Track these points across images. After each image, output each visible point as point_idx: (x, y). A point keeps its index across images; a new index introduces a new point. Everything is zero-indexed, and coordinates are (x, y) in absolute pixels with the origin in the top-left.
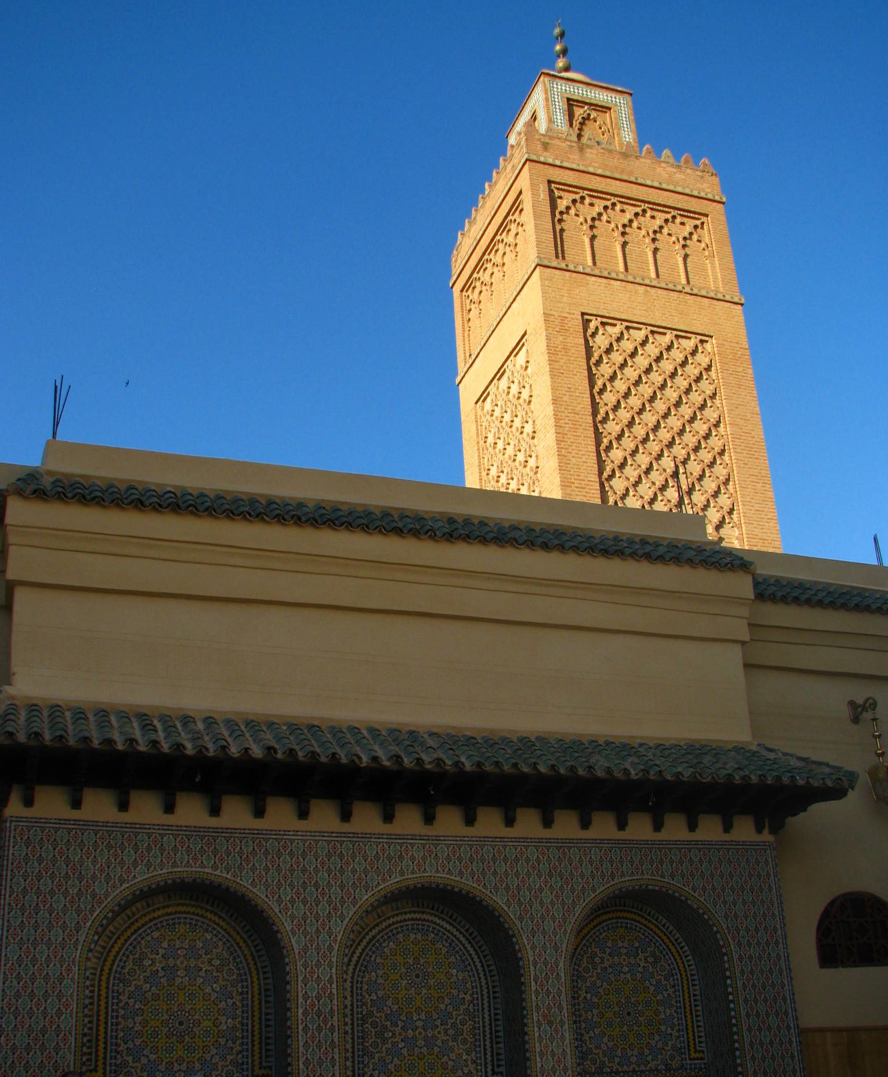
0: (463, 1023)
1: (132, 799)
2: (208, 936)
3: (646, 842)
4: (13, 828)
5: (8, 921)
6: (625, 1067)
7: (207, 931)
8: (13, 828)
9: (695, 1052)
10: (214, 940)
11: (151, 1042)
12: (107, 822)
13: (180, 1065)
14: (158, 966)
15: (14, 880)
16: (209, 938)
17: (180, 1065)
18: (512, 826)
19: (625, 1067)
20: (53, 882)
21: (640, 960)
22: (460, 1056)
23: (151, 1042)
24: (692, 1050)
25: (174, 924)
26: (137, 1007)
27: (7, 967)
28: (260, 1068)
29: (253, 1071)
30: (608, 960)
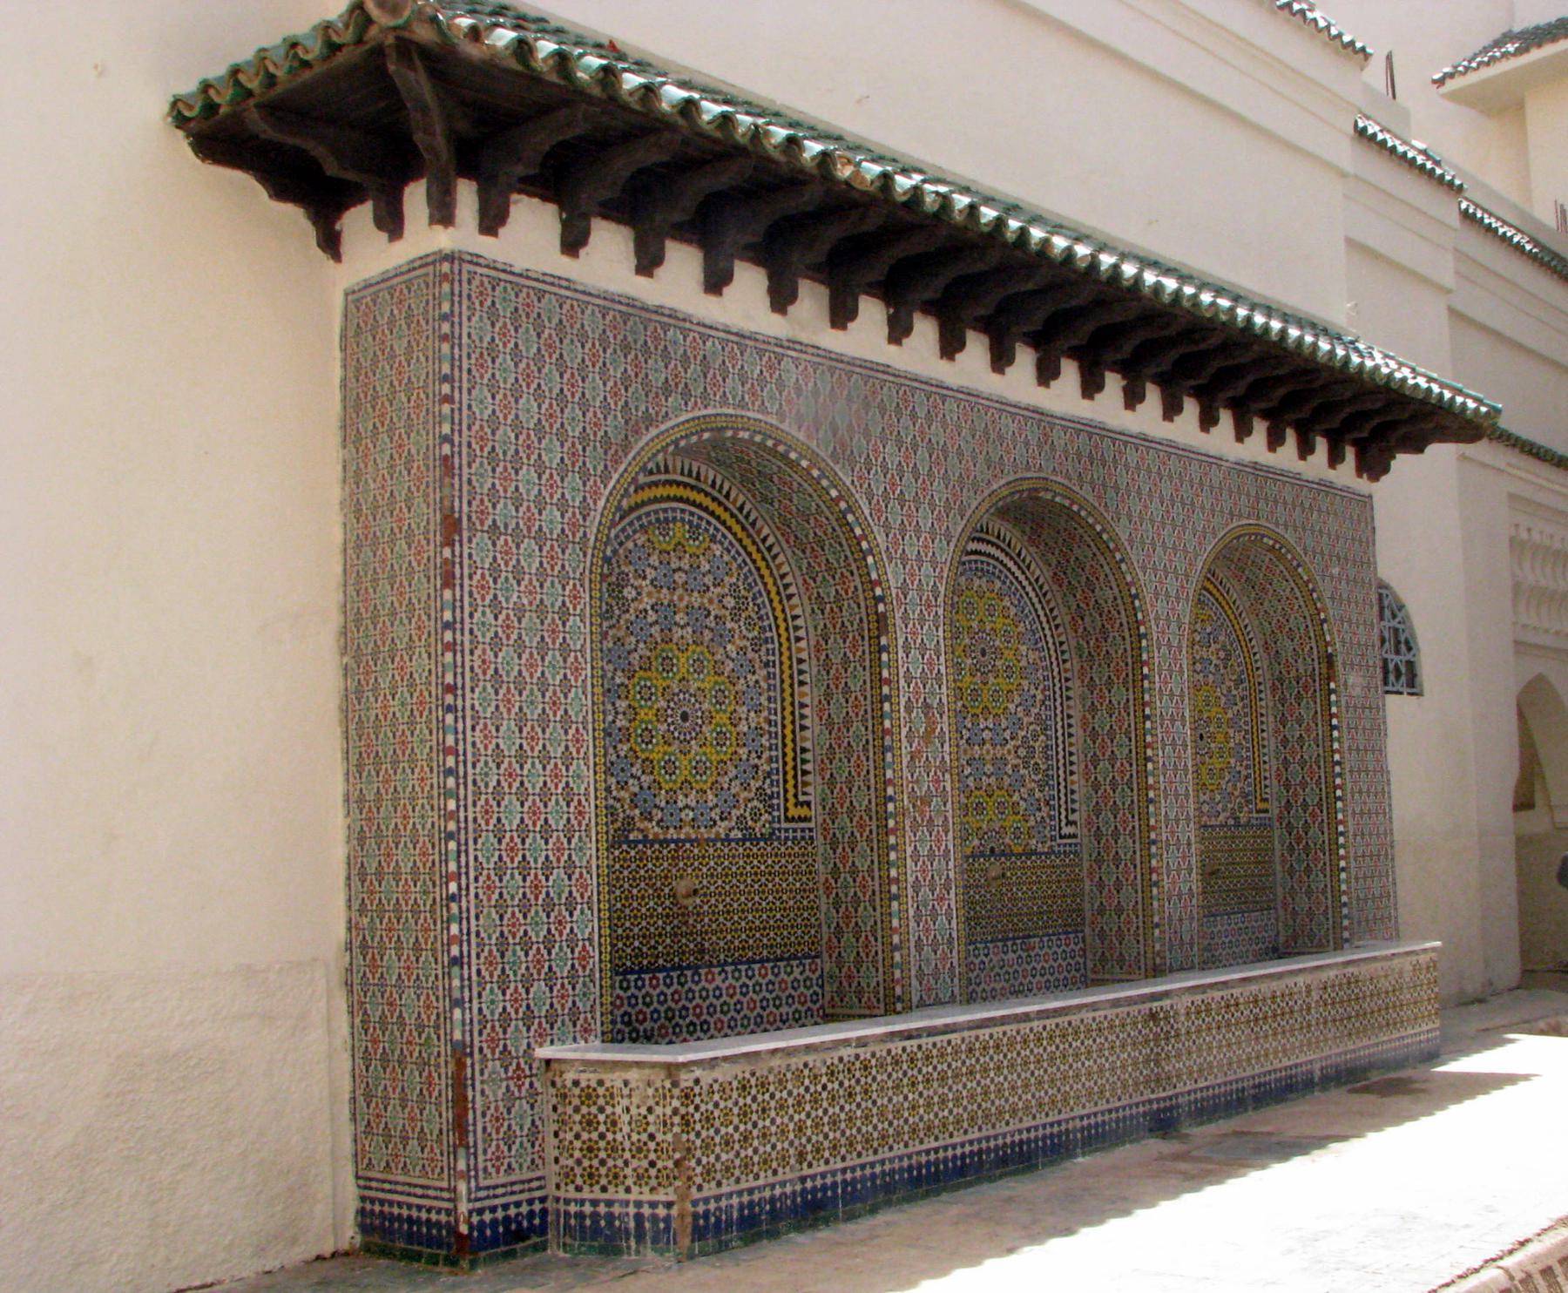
0: (1035, 737)
1: (513, 209)
2: (717, 549)
3: (543, 279)
4: (465, 277)
5: (470, 482)
6: (672, 830)
7: (713, 539)
8: (465, 277)
9: (796, 805)
10: (726, 558)
11: (643, 751)
12: (478, 256)
13: (686, 796)
14: (647, 603)
15: (474, 392)
16: (718, 553)
17: (686, 796)
18: (650, 275)
19: (672, 830)
20: (539, 407)
21: (711, 601)
22: (1031, 792)
23: (643, 751)
24: (792, 800)
25: (666, 520)
26: (618, 681)
27: (474, 583)
28: (796, 805)
29: (786, 809)
30: (649, 595)
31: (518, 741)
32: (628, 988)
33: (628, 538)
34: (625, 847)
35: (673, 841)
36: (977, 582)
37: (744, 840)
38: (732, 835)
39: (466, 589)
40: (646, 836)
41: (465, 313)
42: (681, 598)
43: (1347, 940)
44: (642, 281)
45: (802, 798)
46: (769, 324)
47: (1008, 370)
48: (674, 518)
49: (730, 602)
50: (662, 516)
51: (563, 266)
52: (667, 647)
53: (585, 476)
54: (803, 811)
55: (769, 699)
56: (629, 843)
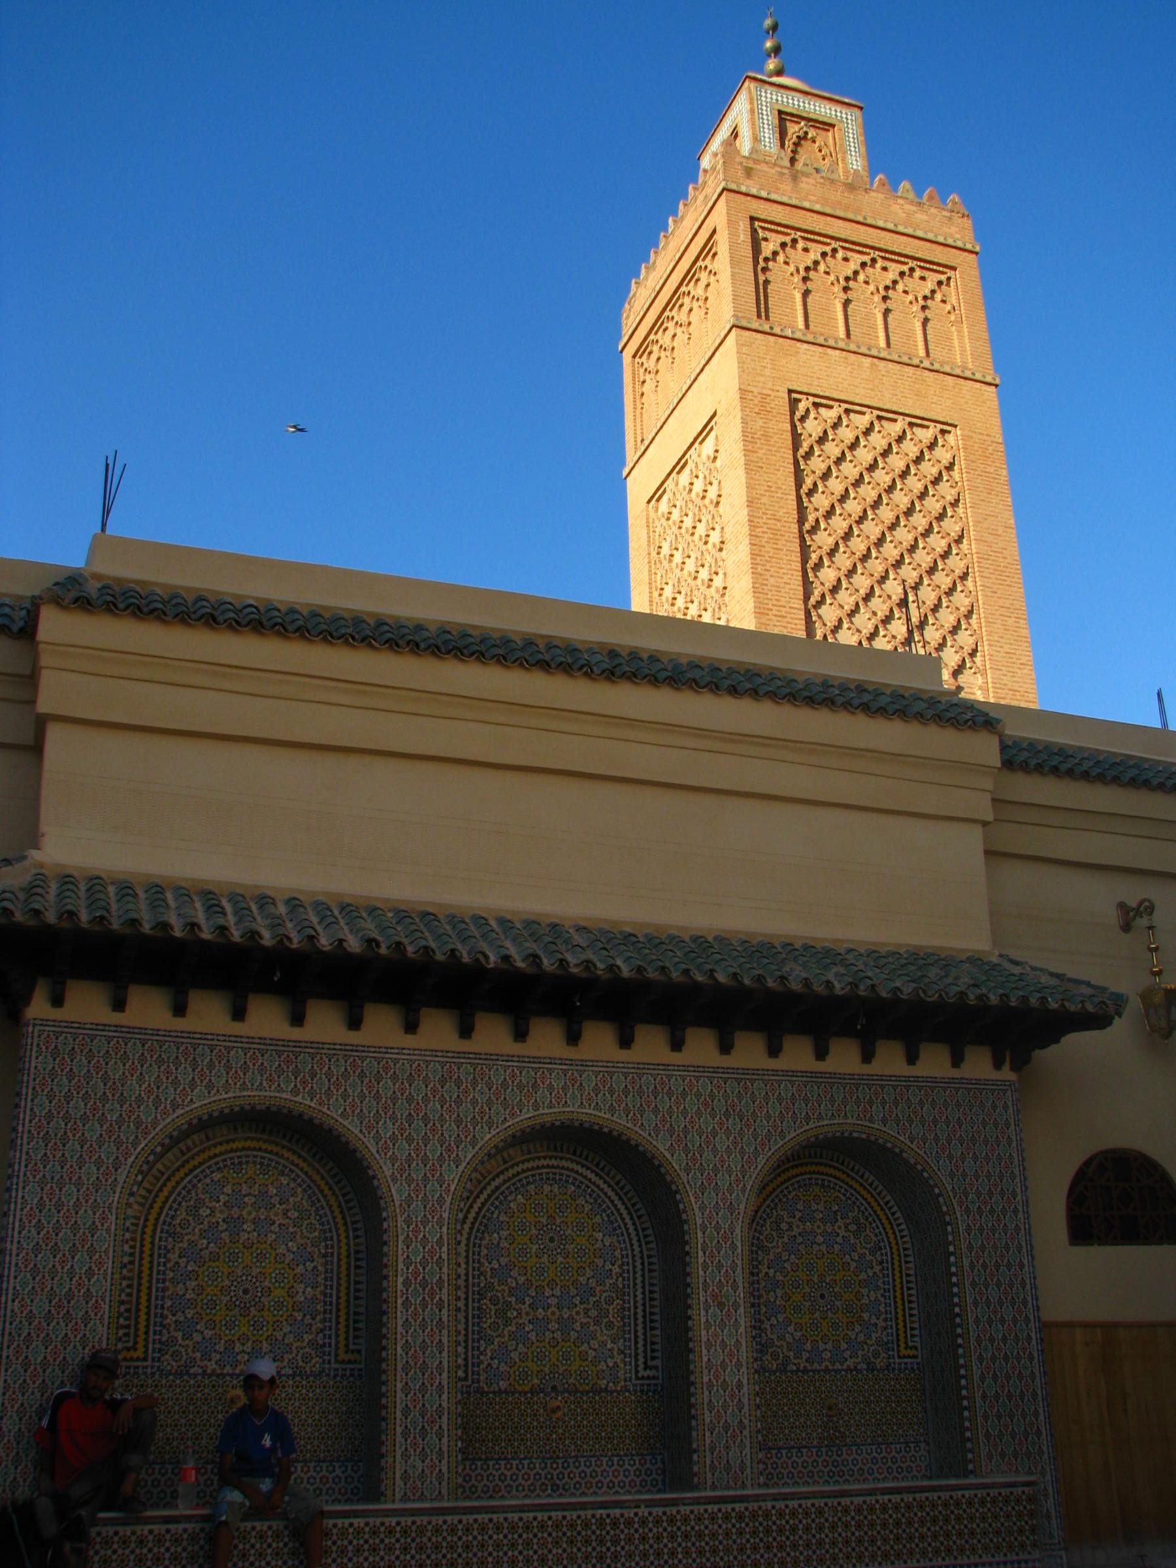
4: (36, 1034)
7: (282, 1173)
8: (36, 1034)
9: (136, 1349)
21: (840, 1227)
26: (190, 1268)
31: (47, 1309)
32: (309, 1471)
33: (205, 1177)
34: (185, 1377)
35: (228, 1374)
36: (547, 1188)
37: (294, 1375)
38: (283, 1372)
39: (18, 1217)
40: (205, 1371)
41: (34, 1054)
42: (249, 1213)
43: (971, 1472)
44: (353, 1033)
45: (910, 1344)
46: (765, 1062)
47: (962, 1066)
48: (247, 1162)
49: (853, 1227)
50: (236, 1161)
51: (866, 1069)
52: (512, 1253)
53: (118, 1144)
54: (911, 1352)
55: (884, 1283)
56: (189, 1375)
